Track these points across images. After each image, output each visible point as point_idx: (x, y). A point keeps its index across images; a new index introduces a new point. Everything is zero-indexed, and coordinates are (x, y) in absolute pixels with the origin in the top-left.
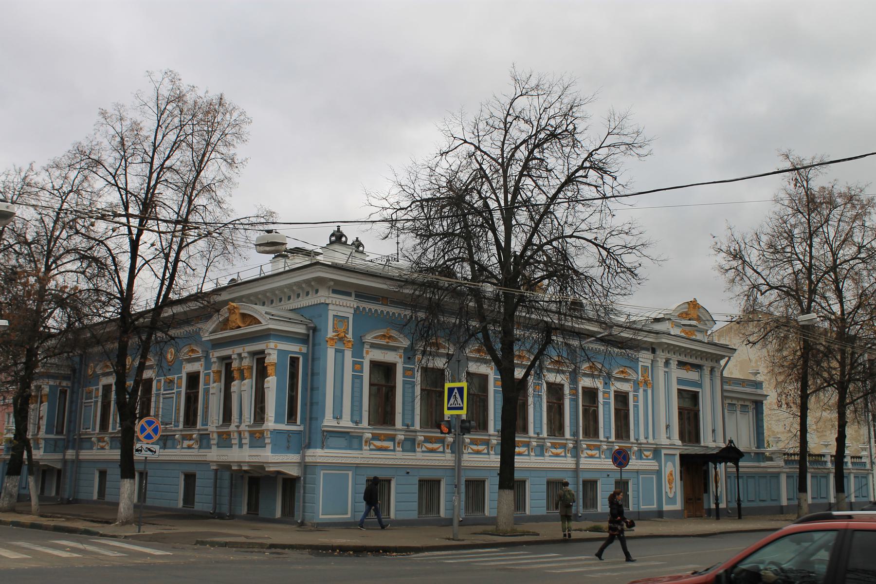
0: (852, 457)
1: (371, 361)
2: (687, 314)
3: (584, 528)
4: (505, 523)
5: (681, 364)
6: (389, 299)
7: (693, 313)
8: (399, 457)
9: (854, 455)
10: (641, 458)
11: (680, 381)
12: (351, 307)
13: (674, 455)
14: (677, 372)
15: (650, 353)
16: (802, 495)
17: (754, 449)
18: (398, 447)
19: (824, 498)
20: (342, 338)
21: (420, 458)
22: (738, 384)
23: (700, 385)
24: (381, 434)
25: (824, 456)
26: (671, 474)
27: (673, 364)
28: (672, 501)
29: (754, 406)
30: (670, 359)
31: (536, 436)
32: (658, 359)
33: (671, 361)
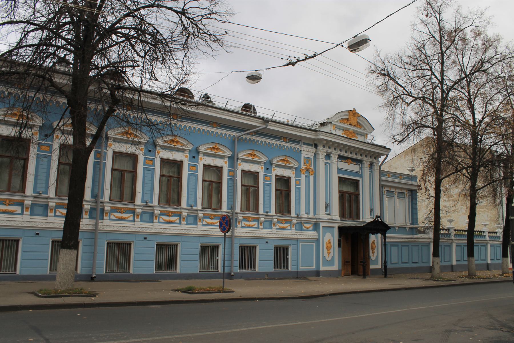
0: (489, 233)
1: (242, 171)
2: (347, 119)
3: (179, 287)
4: (60, 283)
5: (341, 158)
6: (178, 116)
7: (353, 120)
8: (184, 228)
9: (491, 231)
10: (301, 229)
11: (339, 171)
13: (334, 227)
14: (336, 164)
15: (313, 147)
16: (505, 259)
17: (409, 225)
18: (293, 227)
19: (484, 260)
21: (275, 232)
22: (396, 177)
23: (361, 176)
24: (6, 200)
25: (484, 232)
26: (329, 242)
27: (334, 158)
28: (331, 263)
29: (410, 194)
31: (296, 216)
32: (319, 152)
33: (332, 155)
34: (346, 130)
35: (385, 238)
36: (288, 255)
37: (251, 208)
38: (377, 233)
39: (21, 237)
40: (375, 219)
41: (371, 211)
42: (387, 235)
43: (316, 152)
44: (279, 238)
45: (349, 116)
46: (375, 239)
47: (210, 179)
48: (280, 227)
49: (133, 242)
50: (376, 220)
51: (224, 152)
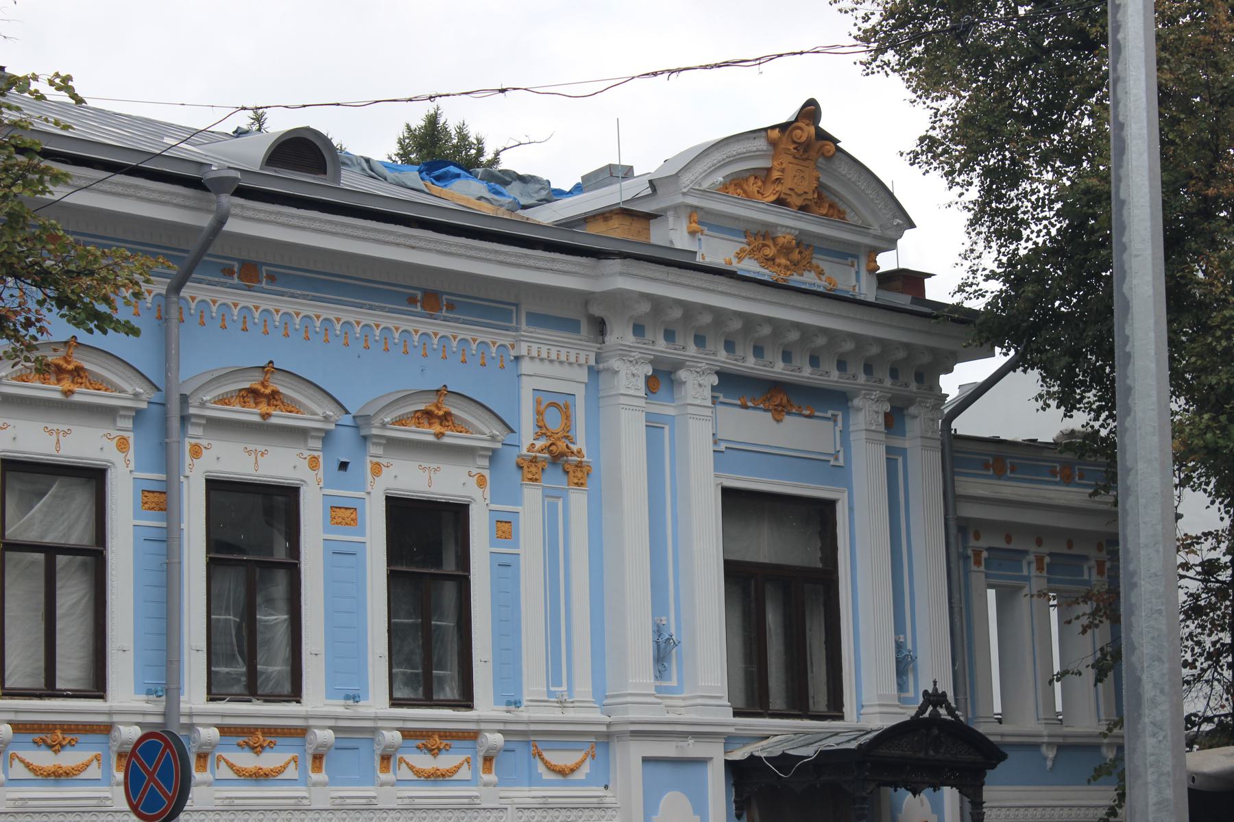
1: (389, 499)
11: (724, 453)
12: (580, 365)
20: (562, 454)
23: (840, 473)
30: (679, 365)
32: (615, 364)
38: (936, 787)
40: (922, 709)
41: (904, 665)
45: (774, 157)
47: (52, 538)
48: (238, 772)
50: (927, 715)
51: (110, 386)
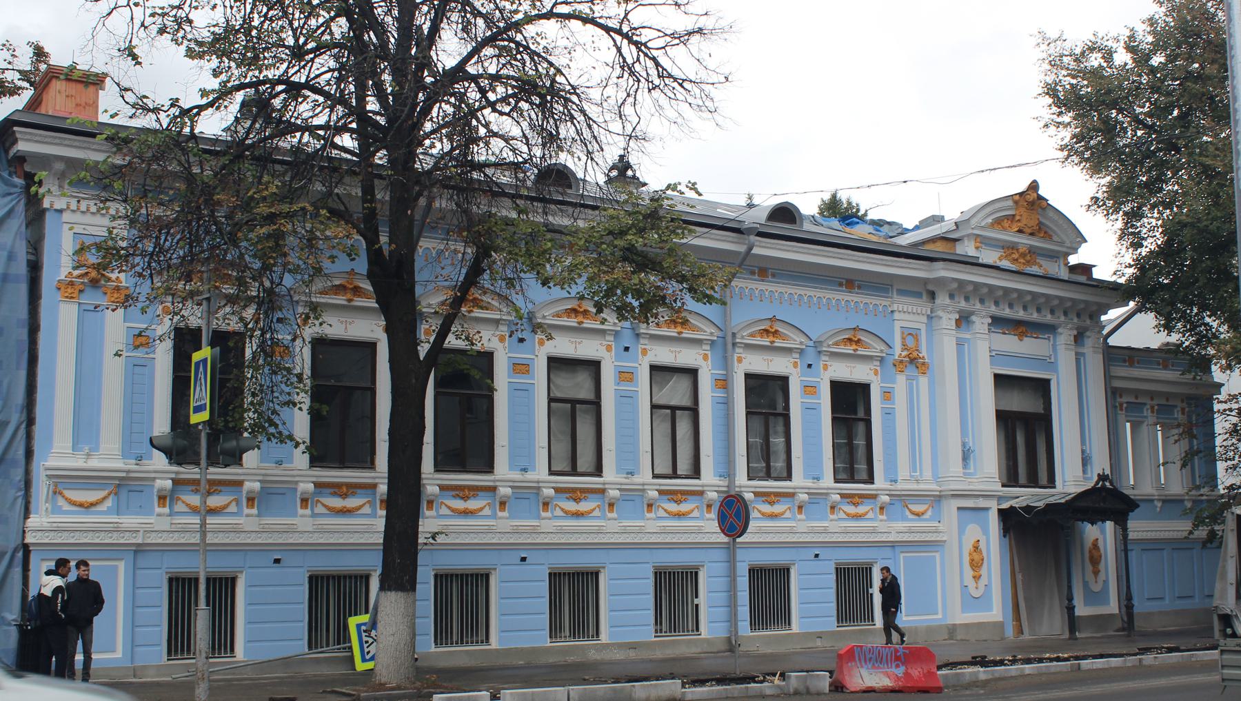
5: (998, 322)
11: (995, 356)
13: (987, 509)
21: (836, 526)
23: (1052, 365)
27: (981, 323)
30: (972, 313)
32: (940, 313)
34: (1009, 248)
35: (1125, 529)
36: (871, 587)
37: (1022, 478)
38: (1103, 521)
39: (375, 568)
40: (1097, 483)
41: (1086, 461)
42: (1131, 524)
43: (931, 312)
44: (112, 544)
45: (1016, 209)
46: (1102, 534)
49: (495, 569)
50: (1099, 486)
